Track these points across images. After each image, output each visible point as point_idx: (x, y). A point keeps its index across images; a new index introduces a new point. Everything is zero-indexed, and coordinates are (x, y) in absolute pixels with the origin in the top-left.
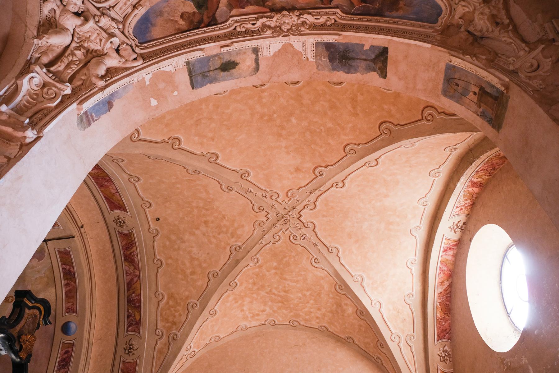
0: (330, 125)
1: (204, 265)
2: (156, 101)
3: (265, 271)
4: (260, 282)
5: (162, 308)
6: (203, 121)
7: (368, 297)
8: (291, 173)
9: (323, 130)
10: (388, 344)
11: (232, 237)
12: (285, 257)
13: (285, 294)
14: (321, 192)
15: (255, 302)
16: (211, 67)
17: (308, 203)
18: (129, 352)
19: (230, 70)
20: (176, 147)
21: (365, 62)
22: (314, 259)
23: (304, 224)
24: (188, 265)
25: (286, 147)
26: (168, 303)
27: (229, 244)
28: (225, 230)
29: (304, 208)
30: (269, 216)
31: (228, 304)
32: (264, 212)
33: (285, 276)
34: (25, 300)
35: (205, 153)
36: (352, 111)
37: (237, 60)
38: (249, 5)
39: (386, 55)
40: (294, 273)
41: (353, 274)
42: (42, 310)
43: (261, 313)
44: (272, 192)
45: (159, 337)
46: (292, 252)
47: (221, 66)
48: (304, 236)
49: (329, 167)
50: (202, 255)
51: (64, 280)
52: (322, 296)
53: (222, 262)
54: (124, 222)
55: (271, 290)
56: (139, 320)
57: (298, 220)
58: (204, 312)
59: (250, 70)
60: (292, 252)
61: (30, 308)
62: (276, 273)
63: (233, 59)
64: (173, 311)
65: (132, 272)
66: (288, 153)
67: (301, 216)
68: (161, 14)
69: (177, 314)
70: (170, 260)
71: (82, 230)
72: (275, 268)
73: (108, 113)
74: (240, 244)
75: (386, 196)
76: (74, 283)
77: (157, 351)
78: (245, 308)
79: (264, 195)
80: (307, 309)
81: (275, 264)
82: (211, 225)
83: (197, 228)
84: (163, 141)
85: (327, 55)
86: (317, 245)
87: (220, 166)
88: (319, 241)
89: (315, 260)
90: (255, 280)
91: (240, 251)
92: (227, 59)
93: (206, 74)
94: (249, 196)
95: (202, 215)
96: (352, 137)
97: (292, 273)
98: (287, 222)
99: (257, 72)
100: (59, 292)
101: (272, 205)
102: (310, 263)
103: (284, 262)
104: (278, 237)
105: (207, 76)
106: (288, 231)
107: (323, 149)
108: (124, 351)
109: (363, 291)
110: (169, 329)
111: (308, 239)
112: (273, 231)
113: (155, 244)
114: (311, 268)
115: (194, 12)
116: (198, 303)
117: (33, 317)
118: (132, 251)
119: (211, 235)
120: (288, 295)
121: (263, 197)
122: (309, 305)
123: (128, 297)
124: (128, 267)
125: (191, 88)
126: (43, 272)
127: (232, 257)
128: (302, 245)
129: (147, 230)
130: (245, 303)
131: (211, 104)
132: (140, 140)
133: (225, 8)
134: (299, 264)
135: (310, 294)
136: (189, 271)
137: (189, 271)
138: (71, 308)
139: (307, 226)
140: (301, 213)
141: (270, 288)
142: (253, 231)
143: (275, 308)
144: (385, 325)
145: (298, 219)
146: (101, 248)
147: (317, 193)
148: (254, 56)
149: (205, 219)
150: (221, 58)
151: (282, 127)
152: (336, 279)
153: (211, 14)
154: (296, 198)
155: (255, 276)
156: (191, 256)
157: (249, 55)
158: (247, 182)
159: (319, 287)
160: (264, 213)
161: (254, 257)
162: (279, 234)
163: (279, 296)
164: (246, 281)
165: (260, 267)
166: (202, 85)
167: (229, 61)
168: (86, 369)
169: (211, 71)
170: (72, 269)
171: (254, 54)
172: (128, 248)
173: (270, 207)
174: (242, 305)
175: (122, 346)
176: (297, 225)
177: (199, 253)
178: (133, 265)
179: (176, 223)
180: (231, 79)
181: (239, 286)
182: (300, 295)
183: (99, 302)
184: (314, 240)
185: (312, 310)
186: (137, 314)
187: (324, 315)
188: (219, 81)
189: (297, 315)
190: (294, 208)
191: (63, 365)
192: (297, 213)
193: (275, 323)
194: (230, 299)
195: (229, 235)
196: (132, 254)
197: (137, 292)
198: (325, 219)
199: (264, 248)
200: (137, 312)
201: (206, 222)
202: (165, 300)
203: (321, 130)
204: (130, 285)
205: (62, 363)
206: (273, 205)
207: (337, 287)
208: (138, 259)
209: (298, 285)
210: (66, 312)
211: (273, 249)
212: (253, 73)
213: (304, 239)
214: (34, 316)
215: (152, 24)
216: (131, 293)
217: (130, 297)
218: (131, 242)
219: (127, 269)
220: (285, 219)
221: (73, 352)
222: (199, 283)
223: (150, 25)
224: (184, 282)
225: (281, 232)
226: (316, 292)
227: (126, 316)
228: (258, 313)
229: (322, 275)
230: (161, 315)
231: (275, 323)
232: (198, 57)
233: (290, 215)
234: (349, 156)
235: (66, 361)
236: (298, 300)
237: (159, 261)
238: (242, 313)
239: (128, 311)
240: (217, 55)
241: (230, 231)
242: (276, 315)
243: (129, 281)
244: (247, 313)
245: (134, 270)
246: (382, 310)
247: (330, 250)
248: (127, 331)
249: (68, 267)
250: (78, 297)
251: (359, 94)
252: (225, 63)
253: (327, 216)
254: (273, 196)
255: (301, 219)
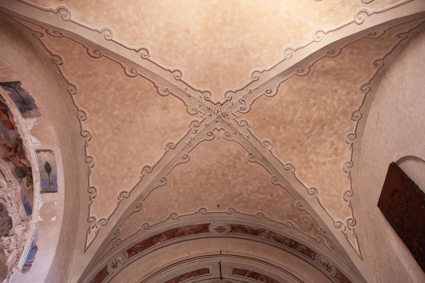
0: (112, 89)
1: (265, 185)
2: (54, 217)
5: (299, 228)
6: (113, 174)
7: (309, 45)
8: (169, 112)
9: (119, 93)
10: (364, 29)
11: (240, 158)
12: (264, 119)
13: (311, 122)
14: (188, 88)
15: (318, 150)
16: (47, 179)
17: (203, 98)
18: (329, 268)
19: (51, 167)
21: (18, 92)
22: (266, 94)
23: (227, 101)
24: (263, 196)
25: (142, 117)
26: (295, 222)
31: (310, 175)
32: (214, 132)
33: (287, 121)
36: (94, 76)
37: (44, 162)
38: (22, 148)
39: (4, 83)
40: (285, 112)
41: (283, 58)
43: (335, 146)
46: (259, 112)
47: (47, 172)
48: (241, 101)
49: (157, 85)
51: (257, 280)
52: (315, 88)
53: (264, 171)
54: (221, 227)
55: (304, 134)
57: (223, 105)
58: (306, 199)
59: (50, 155)
60: (259, 112)
62: (284, 128)
63: (44, 165)
64: (303, 221)
65: (266, 235)
68: (25, 197)
69: (305, 220)
72: (278, 128)
73: (37, 251)
74: (247, 154)
75: (187, 31)
76: (261, 275)
78: (322, 160)
79: (195, 132)
80: (335, 103)
83: (229, 182)
84: (118, 204)
85: (28, 111)
86: (250, 91)
88: (246, 88)
89: (268, 93)
91: (254, 154)
92: (44, 168)
93: (50, 182)
94: (194, 143)
95: (216, 177)
96: (118, 73)
97: (283, 114)
98: (225, 114)
99: (52, 151)
101: (206, 126)
104: (242, 122)
105: (52, 182)
106: (236, 114)
107: (138, 91)
108: (327, 271)
109: (303, 49)
111: (244, 98)
112: (235, 125)
113: (242, 212)
114: (277, 97)
115: (27, 179)
116: (298, 201)
118: (248, 229)
119: (236, 174)
120: (313, 119)
121: (196, 133)
122: (329, 101)
123: (287, 245)
124: (262, 235)
125: (56, 193)
128: (251, 103)
129: (228, 215)
130: (315, 159)
131: (101, 168)
132: (108, 220)
133: (26, 161)
134: (273, 108)
135: (314, 99)
137: (269, 197)
139: (230, 98)
143: (331, 132)
144: (342, 29)
147: (189, 91)
148: (42, 152)
149: (220, 176)
150: (42, 172)
151: (123, 121)
153: (28, 169)
155: (285, 146)
156: (256, 192)
157: (41, 155)
159: (303, 91)
160: (215, 132)
161: (263, 144)
162: (239, 121)
164: (289, 154)
165: (274, 140)
166: (57, 186)
167: (45, 167)
169: (49, 179)
170: (250, 272)
171: (40, 152)
172: (245, 230)
173: (208, 127)
174: (317, 163)
175: (324, 269)
176: (229, 106)
177: (253, 186)
178: (261, 232)
179: (223, 195)
180: (56, 167)
181: (292, 162)
183: (288, 265)
184: (245, 92)
185: (336, 98)
187: (344, 87)
188: (56, 175)
189: (344, 113)
192: (216, 106)
193: (353, 134)
194: (304, 172)
195: (237, 161)
196: (251, 229)
198: (221, 83)
199: (254, 135)
200: (300, 246)
201: (224, 175)
202: (293, 223)
204: (277, 240)
206: (206, 125)
208: (256, 228)
209: (301, 109)
211: (256, 127)
212: (52, 153)
213: (244, 101)
215: (28, 204)
217: (288, 244)
218: (240, 227)
219: (264, 236)
222: (281, 193)
223: (28, 205)
224: (279, 204)
225: (237, 119)
227: (302, 254)
231: (353, 134)
232: (40, 185)
233: (218, 112)
236: (321, 111)
237: (258, 214)
238: (328, 164)
239: (299, 251)
240: (41, 174)
241: (233, 159)
242: (340, 132)
245: (265, 233)
246: (326, 30)
248: (314, 260)
250: (273, 278)
251: (77, 74)
252: (46, 170)
253: (218, 81)
254: (196, 125)
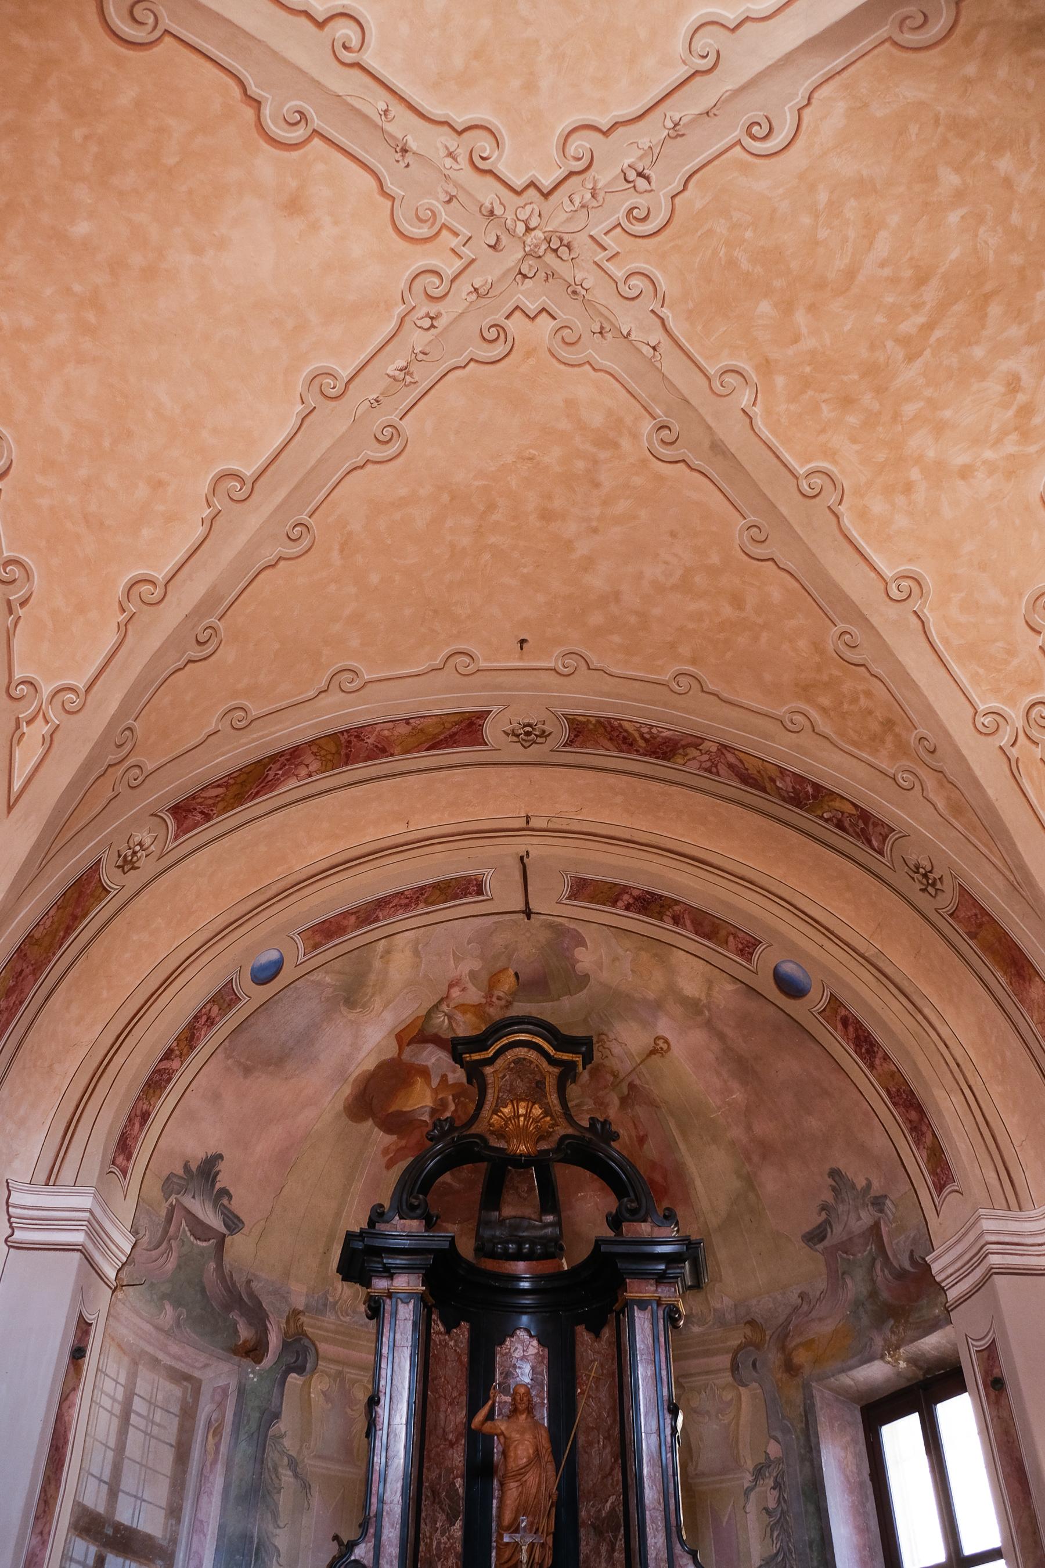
1: (715, 559)
3: (790, 351)
4: (845, 378)
5: (835, 733)
8: (315, 227)
11: (616, 445)
12: (732, 263)
13: (934, 282)
14: (397, 110)
15: (947, 414)
18: (933, 885)
20: (158, 593)
22: (747, 142)
23: (572, 174)
24: (702, 605)
25: (198, 250)
26: (824, 710)
27: (644, 462)
28: (580, 465)
29: (490, 172)
30: (532, 307)
31: (901, 521)
32: (509, 324)
34: (468, 1059)
35: (207, 512)
40: (823, 234)
42: (530, 1039)
43: (1021, 398)
44: (407, 294)
45: (918, 787)
46: (710, 232)
48: (632, 175)
49: (254, 90)
50: (676, 555)
51: (662, 920)
52: (972, 112)
55: (897, 340)
56: (857, 810)
57: (551, 198)
58: (875, 620)
60: (710, 232)
61: (490, 1061)
65: (706, 757)
66: (222, 244)
67: (532, 184)
69: (863, 701)
70: (680, 650)
71: (534, 823)
72: (787, 308)
74: (647, 426)
77: (954, 817)
79: (427, 323)
81: (765, 307)
82: (557, 504)
83: (569, 545)
84: (123, 628)
87: (272, 468)
89: (754, 138)
90: (825, 396)
91: (676, 427)
94: (424, 374)
98: (561, 240)
100: (692, 947)
101: (474, 296)
102: (773, 160)
103: (759, 270)
104: (634, 281)
106: (607, 240)
110: (902, 748)
111: (647, 161)
112: (602, 295)
114: (796, 159)
117: (511, 1070)
118: (636, 735)
119: (597, 511)
121: (432, 326)
123: (784, 799)
124: (689, 760)
126: (620, 951)
127: (696, 463)
128: (676, 185)
130: (931, 454)
135: (957, 170)
136: (728, 611)
137: (728, 611)
138: (742, 944)
140: (519, 183)
141: (890, 344)
142: (594, 369)
143: (1015, 331)
145: (546, 195)
146: (619, 799)
152: (865, 44)
154: (440, 207)
155: (810, 393)
158: (357, 380)
159: (913, 129)
160: (516, 325)
161: (716, 385)
162: (619, 274)
163: (942, 307)
164: (823, 431)
165: (766, 367)
168: (927, 1011)
170: (636, 893)
172: (625, 738)
173: (483, 302)
175: (913, 888)
176: (577, 203)
177: (666, 563)
178: (684, 747)
179: (541, 598)
181: (835, 462)
182: (953, 218)
186: (837, 804)
190: (492, 213)
191: (868, 1051)
192: (520, 201)
194: (878, 506)
195: (603, 455)
196: (647, 736)
197: (774, 773)
199: (683, 341)
201: (546, 515)
202: (814, 714)
203: (86, 138)
204: (746, 779)
205: (863, 1050)
206: (476, 290)
207: (909, 38)
210: (749, 960)
211: (691, 305)
213: (647, 178)
214: (512, 1065)
216: (774, 788)
217: (786, 795)
219: (695, 764)
220: (544, 246)
221: (853, 1010)
222: (776, 595)
224: (765, 636)
225: (609, 266)
226: (945, 142)
228: (1014, 407)
229: (841, 107)
230: (854, 744)
233: (528, 230)
234: (166, 22)
235: (862, 1038)
238: (980, 475)
239: (827, 820)
243: (736, 775)
244: (989, 454)
245: (701, 750)
247: (705, 64)
249: (626, 897)
250: (718, 915)
255: (546, 183)
